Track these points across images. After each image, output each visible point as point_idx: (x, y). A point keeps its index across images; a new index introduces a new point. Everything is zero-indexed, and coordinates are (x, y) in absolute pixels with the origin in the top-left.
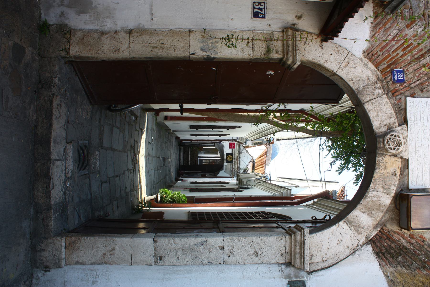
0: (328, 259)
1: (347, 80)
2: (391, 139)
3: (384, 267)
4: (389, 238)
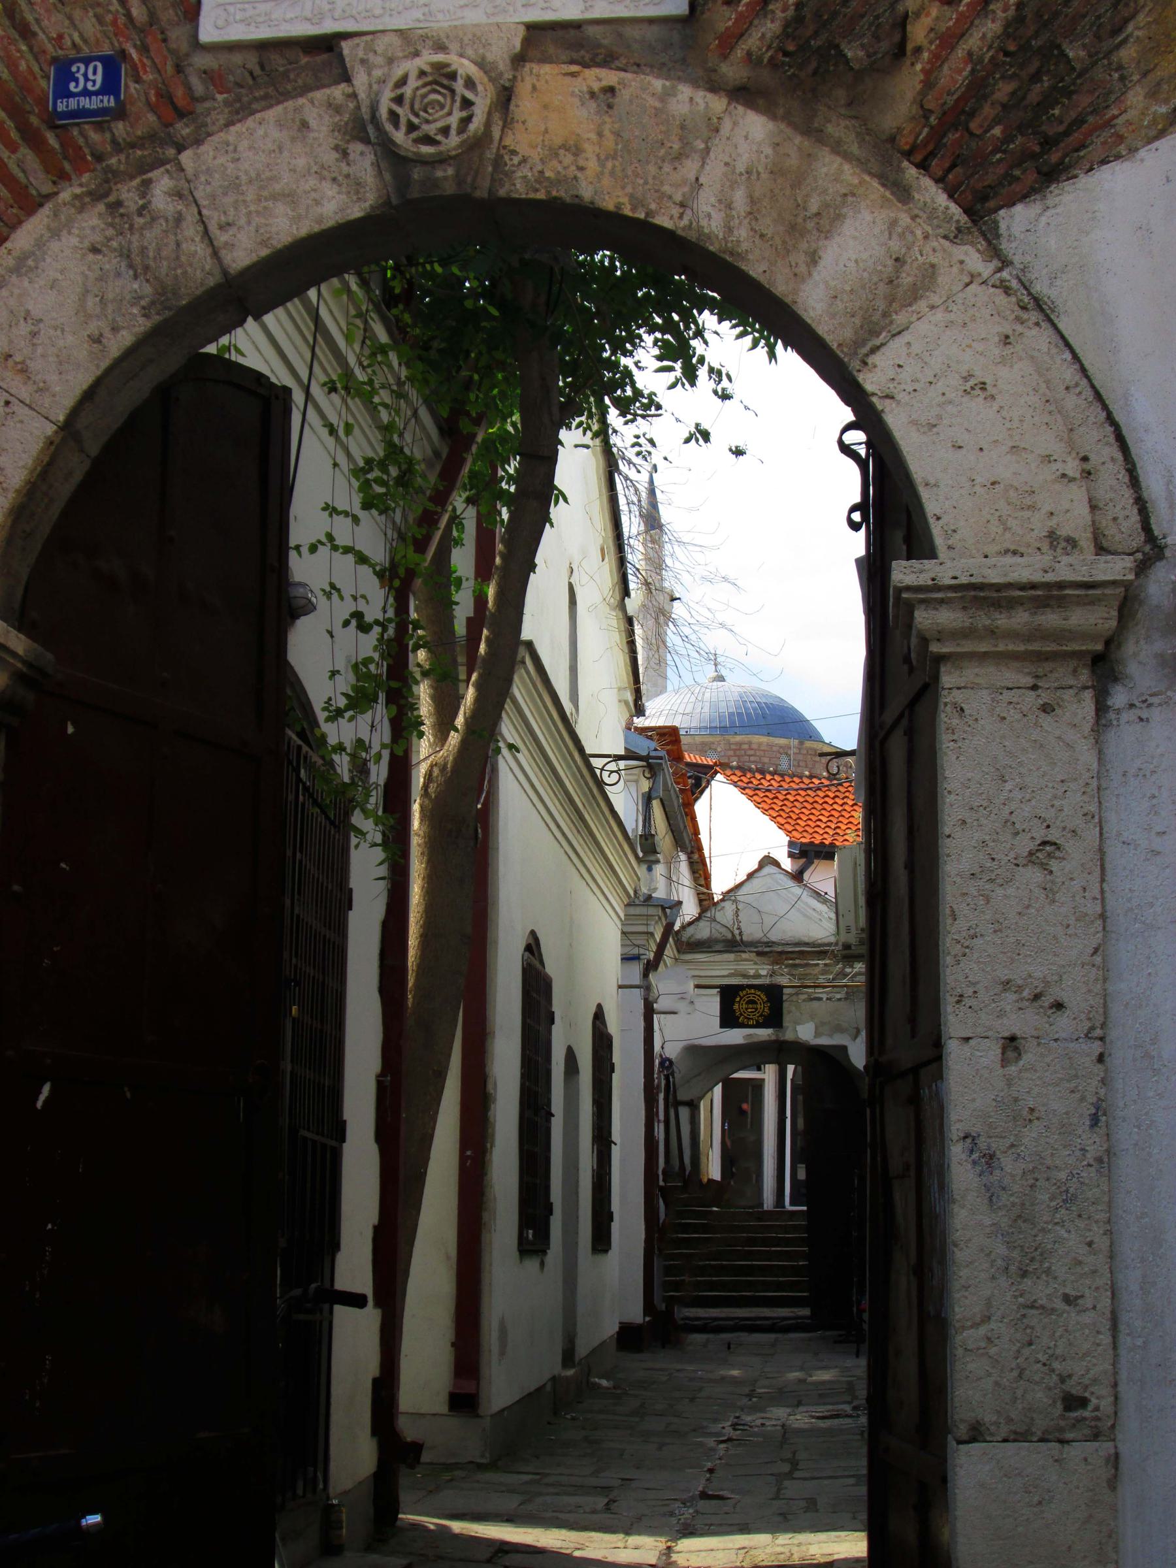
0: (1071, 445)
1: (98, 366)
2: (416, 121)
3: (1121, 138)
4: (963, 112)
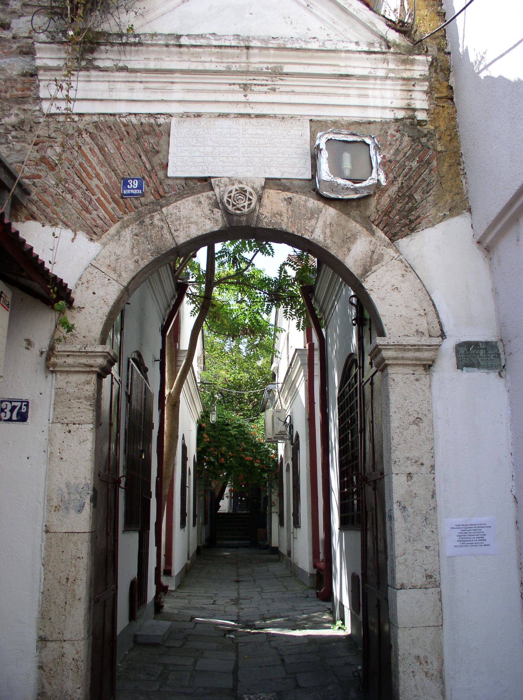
2: (235, 204)
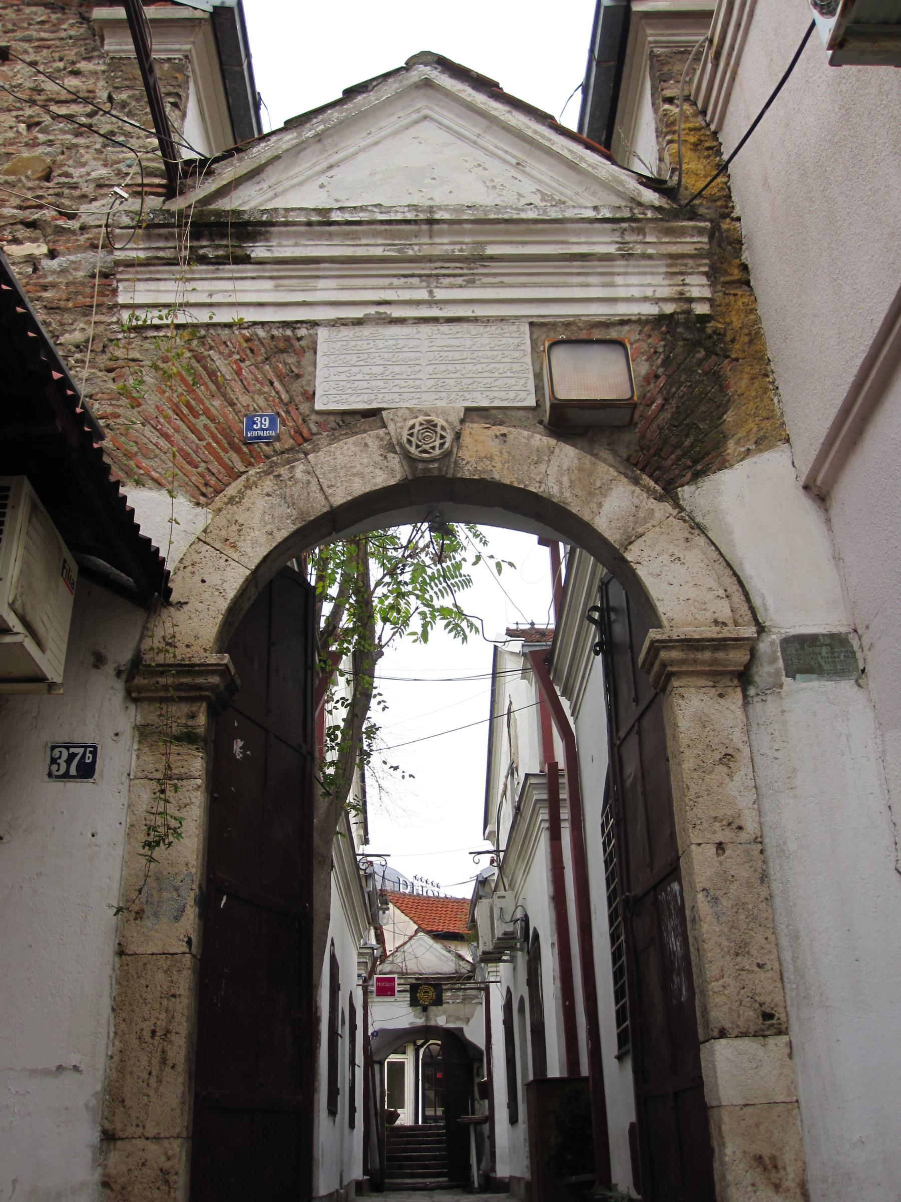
0: (721, 585)
